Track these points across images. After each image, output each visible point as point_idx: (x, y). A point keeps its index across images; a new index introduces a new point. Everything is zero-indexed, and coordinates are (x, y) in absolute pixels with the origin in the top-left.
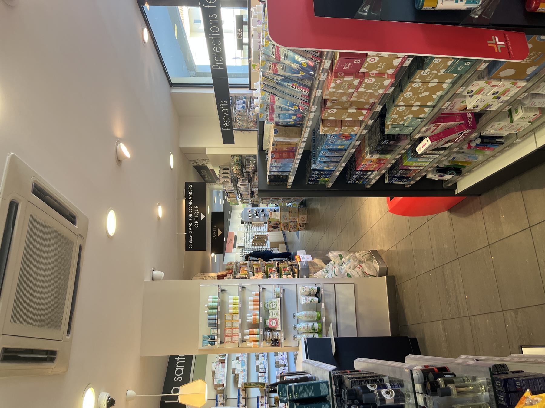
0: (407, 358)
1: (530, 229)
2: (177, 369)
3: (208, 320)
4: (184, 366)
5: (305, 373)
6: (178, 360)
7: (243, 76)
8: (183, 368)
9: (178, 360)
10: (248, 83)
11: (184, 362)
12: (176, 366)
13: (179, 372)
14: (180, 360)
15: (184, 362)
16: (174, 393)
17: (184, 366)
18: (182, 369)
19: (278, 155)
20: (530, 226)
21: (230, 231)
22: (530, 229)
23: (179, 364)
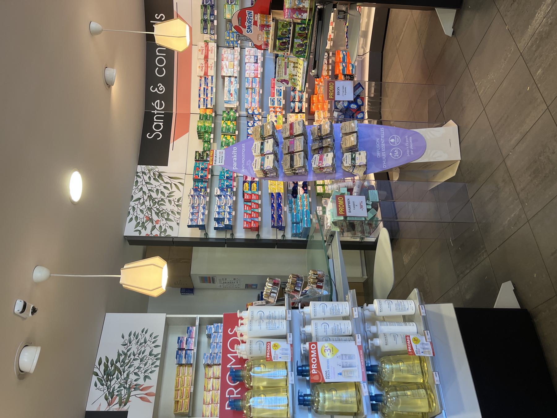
0: (377, 191)
1: (529, 223)
2: (155, 123)
3: (186, 37)
4: (163, 121)
5: (289, 187)
6: (156, 113)
7: (192, 337)
8: (162, 123)
9: (156, 113)
10: (208, 107)
11: (163, 116)
12: (156, 53)
13: (161, 62)
14: (158, 114)
15: (163, 116)
16: (159, 53)
17: (163, 121)
18: (161, 124)
19: (270, 26)
20: (528, 219)
21: (200, 235)
22: (529, 223)
23: (157, 118)
